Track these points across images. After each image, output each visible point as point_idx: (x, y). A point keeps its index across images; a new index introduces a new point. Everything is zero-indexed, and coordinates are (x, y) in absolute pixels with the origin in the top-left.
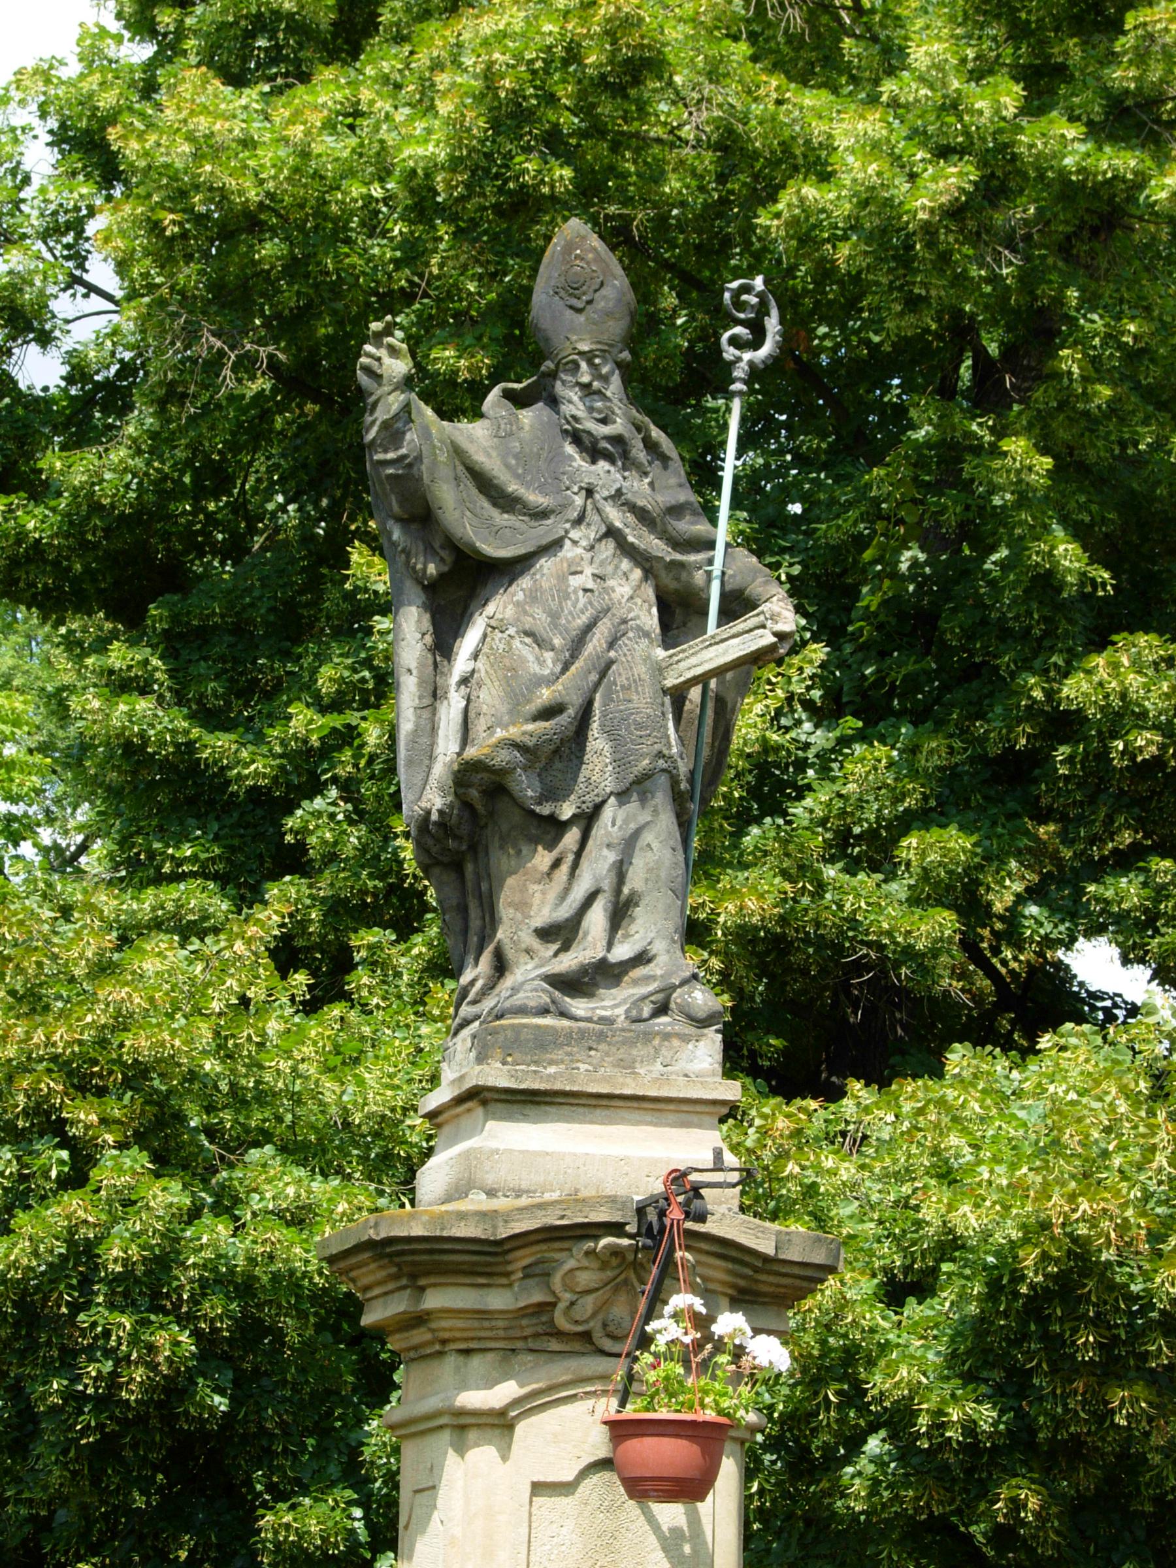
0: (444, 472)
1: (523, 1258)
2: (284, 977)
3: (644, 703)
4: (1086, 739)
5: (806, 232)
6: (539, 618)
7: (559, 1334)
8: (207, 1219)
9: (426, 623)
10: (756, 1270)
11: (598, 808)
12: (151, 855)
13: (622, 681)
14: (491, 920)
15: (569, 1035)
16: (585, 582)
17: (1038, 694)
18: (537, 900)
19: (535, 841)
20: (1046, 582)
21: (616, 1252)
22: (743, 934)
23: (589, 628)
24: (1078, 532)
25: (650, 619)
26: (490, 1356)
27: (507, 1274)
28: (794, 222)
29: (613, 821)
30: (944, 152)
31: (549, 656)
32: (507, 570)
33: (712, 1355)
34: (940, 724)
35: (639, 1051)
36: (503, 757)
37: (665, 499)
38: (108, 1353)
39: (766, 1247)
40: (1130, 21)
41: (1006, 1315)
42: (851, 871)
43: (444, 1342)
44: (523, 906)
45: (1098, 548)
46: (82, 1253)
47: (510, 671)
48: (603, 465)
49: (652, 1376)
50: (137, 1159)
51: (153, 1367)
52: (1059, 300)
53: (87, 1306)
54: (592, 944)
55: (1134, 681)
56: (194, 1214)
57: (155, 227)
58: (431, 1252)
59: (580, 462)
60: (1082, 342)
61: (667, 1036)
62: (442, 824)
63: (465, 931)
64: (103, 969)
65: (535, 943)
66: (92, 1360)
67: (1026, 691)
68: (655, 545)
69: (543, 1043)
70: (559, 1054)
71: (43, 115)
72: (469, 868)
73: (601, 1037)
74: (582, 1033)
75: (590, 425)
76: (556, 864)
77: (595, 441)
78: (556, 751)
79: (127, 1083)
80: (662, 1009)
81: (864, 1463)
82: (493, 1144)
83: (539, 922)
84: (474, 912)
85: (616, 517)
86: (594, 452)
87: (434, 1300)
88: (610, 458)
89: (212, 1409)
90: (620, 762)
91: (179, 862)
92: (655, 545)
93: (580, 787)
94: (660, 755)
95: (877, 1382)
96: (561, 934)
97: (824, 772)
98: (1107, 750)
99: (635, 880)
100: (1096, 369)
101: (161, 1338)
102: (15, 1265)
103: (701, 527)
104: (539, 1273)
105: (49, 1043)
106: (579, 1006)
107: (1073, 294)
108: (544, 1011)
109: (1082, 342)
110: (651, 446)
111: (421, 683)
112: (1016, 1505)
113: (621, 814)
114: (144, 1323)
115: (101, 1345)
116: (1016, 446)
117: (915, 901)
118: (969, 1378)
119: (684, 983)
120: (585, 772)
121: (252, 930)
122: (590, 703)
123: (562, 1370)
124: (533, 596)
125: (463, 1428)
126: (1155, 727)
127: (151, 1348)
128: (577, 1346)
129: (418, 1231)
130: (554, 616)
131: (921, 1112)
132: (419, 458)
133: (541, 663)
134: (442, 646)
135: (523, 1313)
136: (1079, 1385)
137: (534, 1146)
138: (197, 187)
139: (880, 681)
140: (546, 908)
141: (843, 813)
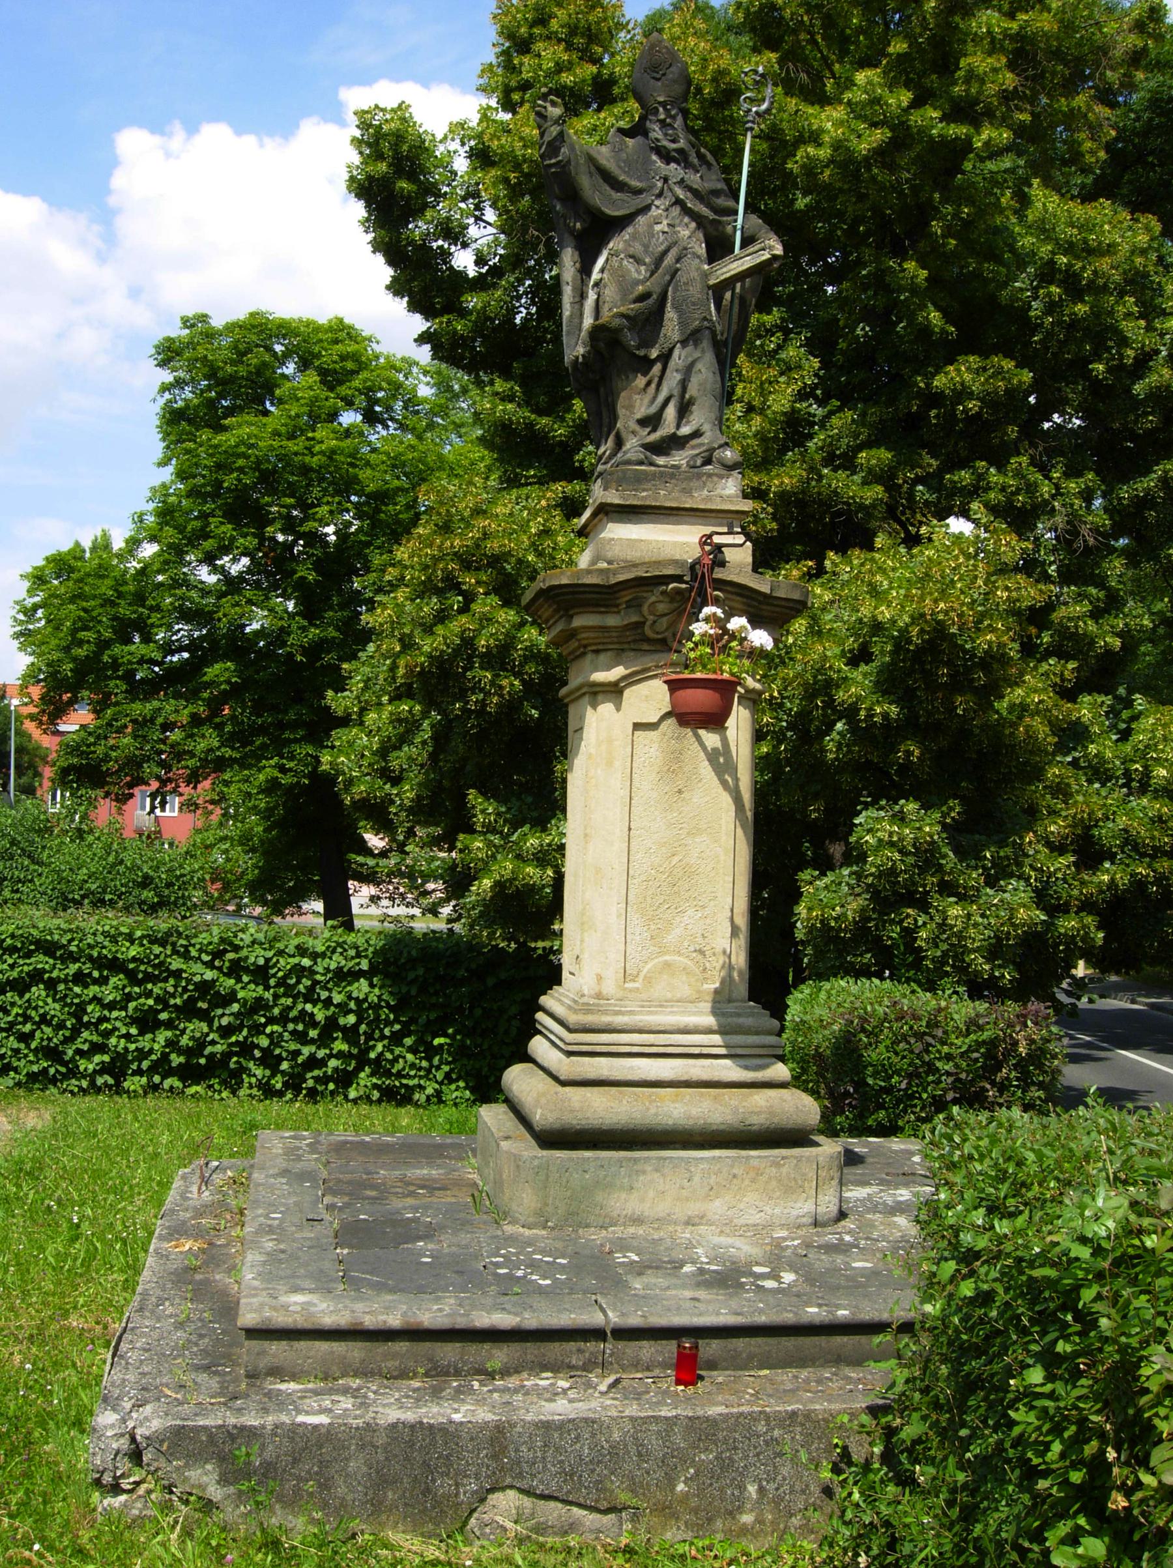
0: (583, 169)
1: (626, 596)
2: (568, 520)
3: (695, 291)
4: (945, 406)
5: (810, 169)
6: (638, 248)
7: (648, 640)
8: (527, 627)
9: (577, 257)
10: (760, 602)
11: (671, 350)
12: (516, 475)
13: (684, 280)
14: (614, 418)
15: (654, 476)
16: (663, 225)
17: (922, 385)
18: (638, 403)
19: (636, 371)
20: (925, 330)
21: (678, 591)
22: (783, 495)
23: (665, 253)
24: (938, 308)
25: (702, 249)
26: (609, 653)
27: (617, 606)
28: (804, 166)
29: (679, 357)
30: (874, 125)
31: (643, 268)
32: (620, 223)
33: (729, 642)
34: (876, 403)
35: (695, 483)
36: (617, 322)
37: (709, 185)
38: (482, 690)
39: (765, 588)
40: (962, 63)
41: (903, 661)
42: (835, 470)
43: (585, 646)
44: (630, 407)
45: (947, 316)
46: (468, 642)
47: (621, 277)
48: (673, 165)
49: (692, 655)
50: (494, 600)
51: (501, 696)
52: (931, 199)
53: (471, 668)
54: (668, 426)
55: (967, 377)
56: (523, 624)
57: (506, 180)
58: (573, 593)
59: (659, 163)
60: (943, 218)
61: (710, 475)
62: (585, 364)
63: (601, 426)
64: (478, 512)
65: (637, 428)
66: (474, 693)
67: (916, 384)
68: (705, 211)
69: (639, 480)
70: (649, 486)
71: (463, 144)
72: (602, 390)
73: (672, 476)
74: (662, 474)
75: (665, 143)
76: (649, 384)
77: (668, 151)
78: (647, 320)
79: (489, 565)
80: (708, 461)
81: (834, 735)
82: (611, 536)
83: (638, 416)
84: (605, 414)
85: (681, 193)
86: (667, 157)
87: (577, 622)
88: (678, 162)
89: (531, 716)
90: (682, 323)
91: (527, 478)
92: (705, 211)
93: (662, 339)
94: (705, 319)
95: (840, 695)
96: (652, 421)
97: (823, 426)
98: (954, 410)
99: (693, 390)
100: (948, 232)
101: (505, 682)
102: (436, 649)
103: (730, 203)
104: (635, 604)
105: (452, 546)
106: (661, 461)
107: (937, 195)
108: (641, 463)
109: (943, 218)
110: (701, 157)
111: (574, 289)
112: (909, 753)
113: (684, 353)
114: (498, 676)
115: (477, 687)
116: (910, 265)
117: (865, 483)
118: (885, 693)
119: (721, 446)
120: (663, 331)
121: (549, 494)
122: (666, 292)
123: (649, 661)
124: (634, 237)
125: (595, 694)
126: (978, 399)
127: (501, 687)
128: (659, 647)
129: (565, 581)
130: (646, 247)
131: (862, 565)
132: (569, 162)
133: (639, 272)
134: (585, 269)
135: (627, 627)
136: (940, 695)
137: (634, 537)
138: (525, 161)
139: (848, 382)
140: (643, 409)
141: (831, 444)
